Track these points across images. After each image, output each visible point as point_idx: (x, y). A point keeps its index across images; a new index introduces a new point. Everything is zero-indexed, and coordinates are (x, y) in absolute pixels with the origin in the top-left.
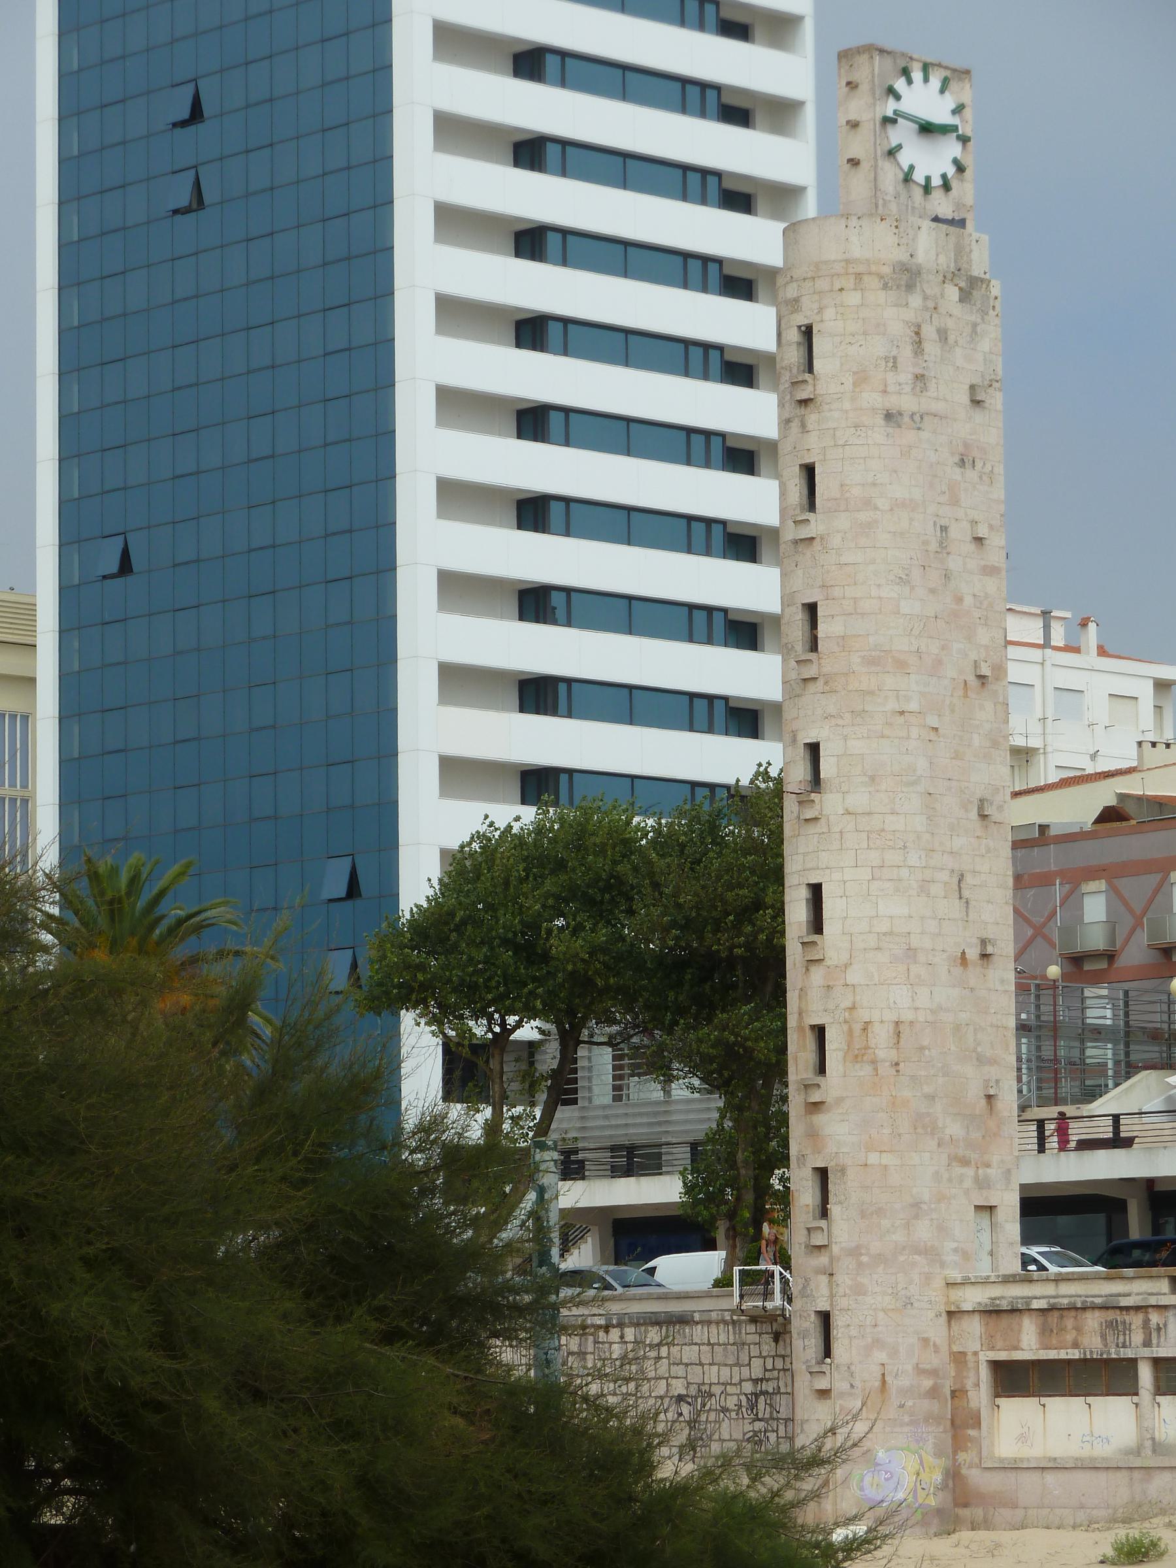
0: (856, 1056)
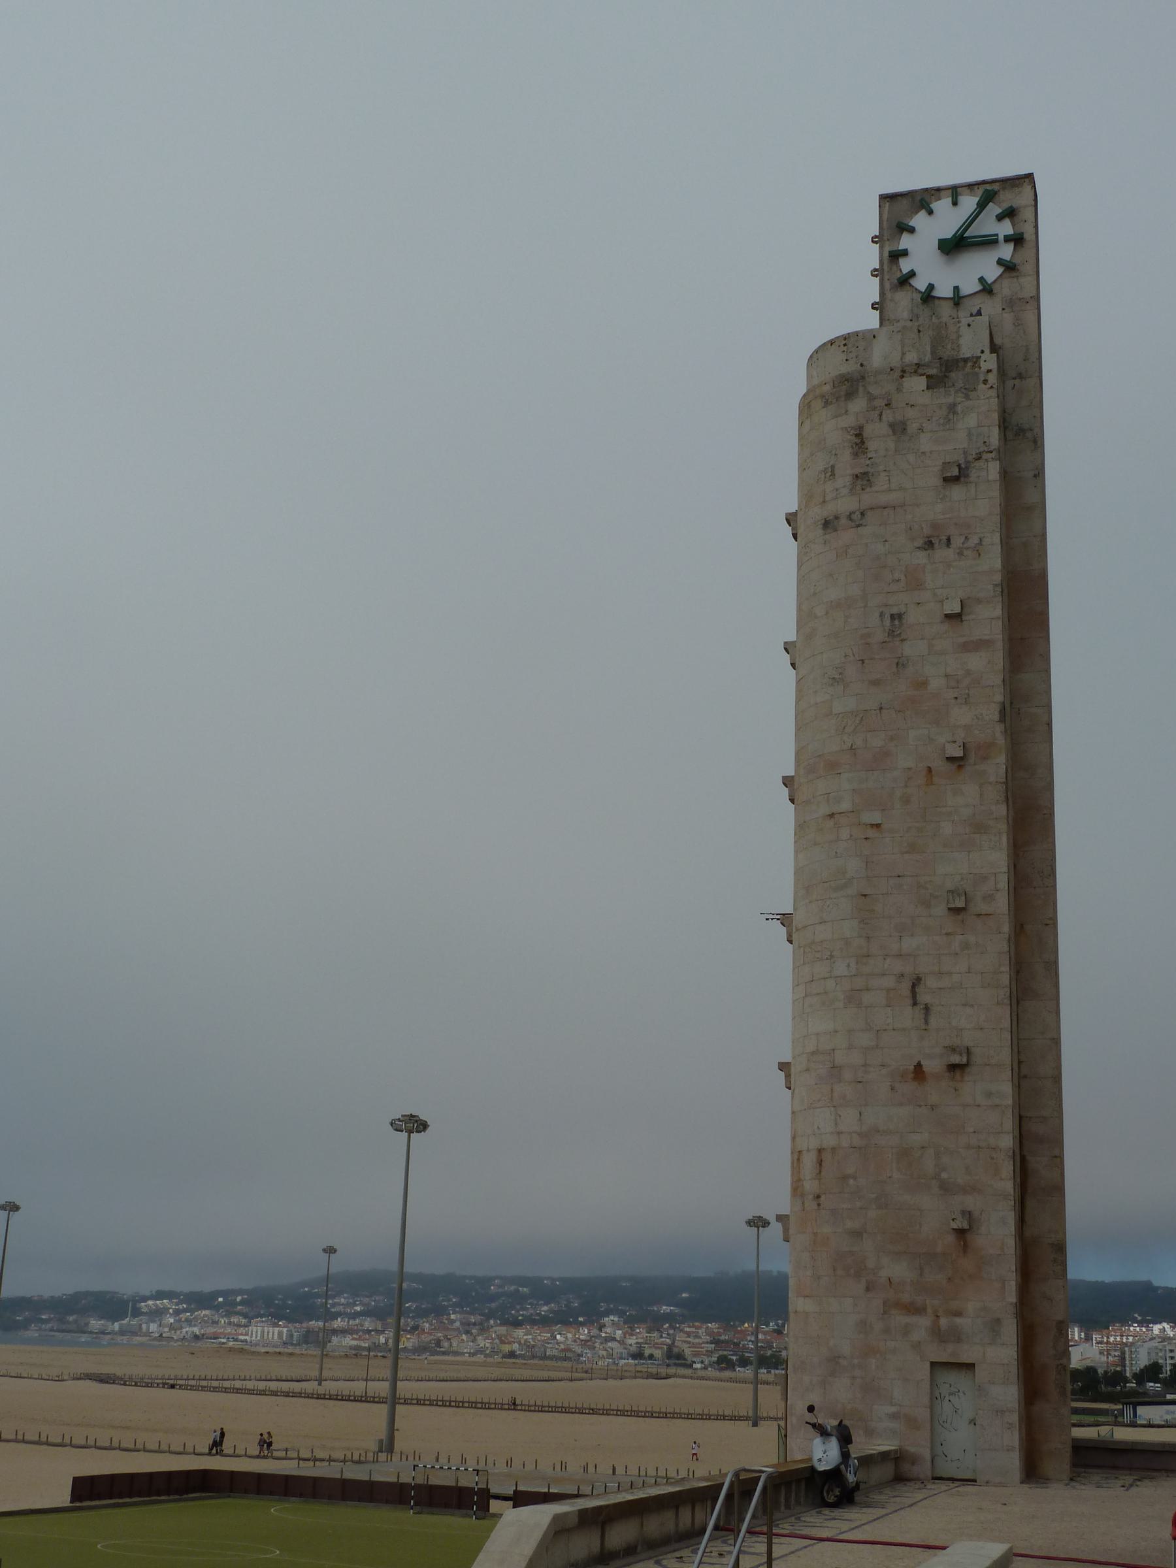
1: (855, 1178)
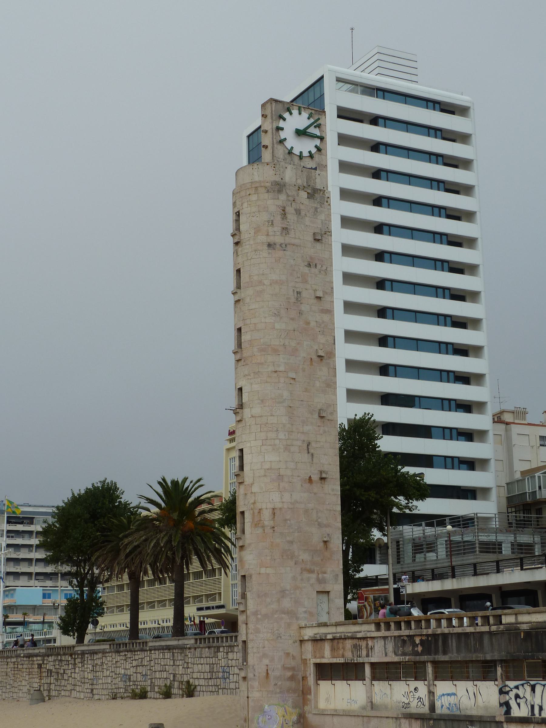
0: (256, 525)
1: (290, 520)
